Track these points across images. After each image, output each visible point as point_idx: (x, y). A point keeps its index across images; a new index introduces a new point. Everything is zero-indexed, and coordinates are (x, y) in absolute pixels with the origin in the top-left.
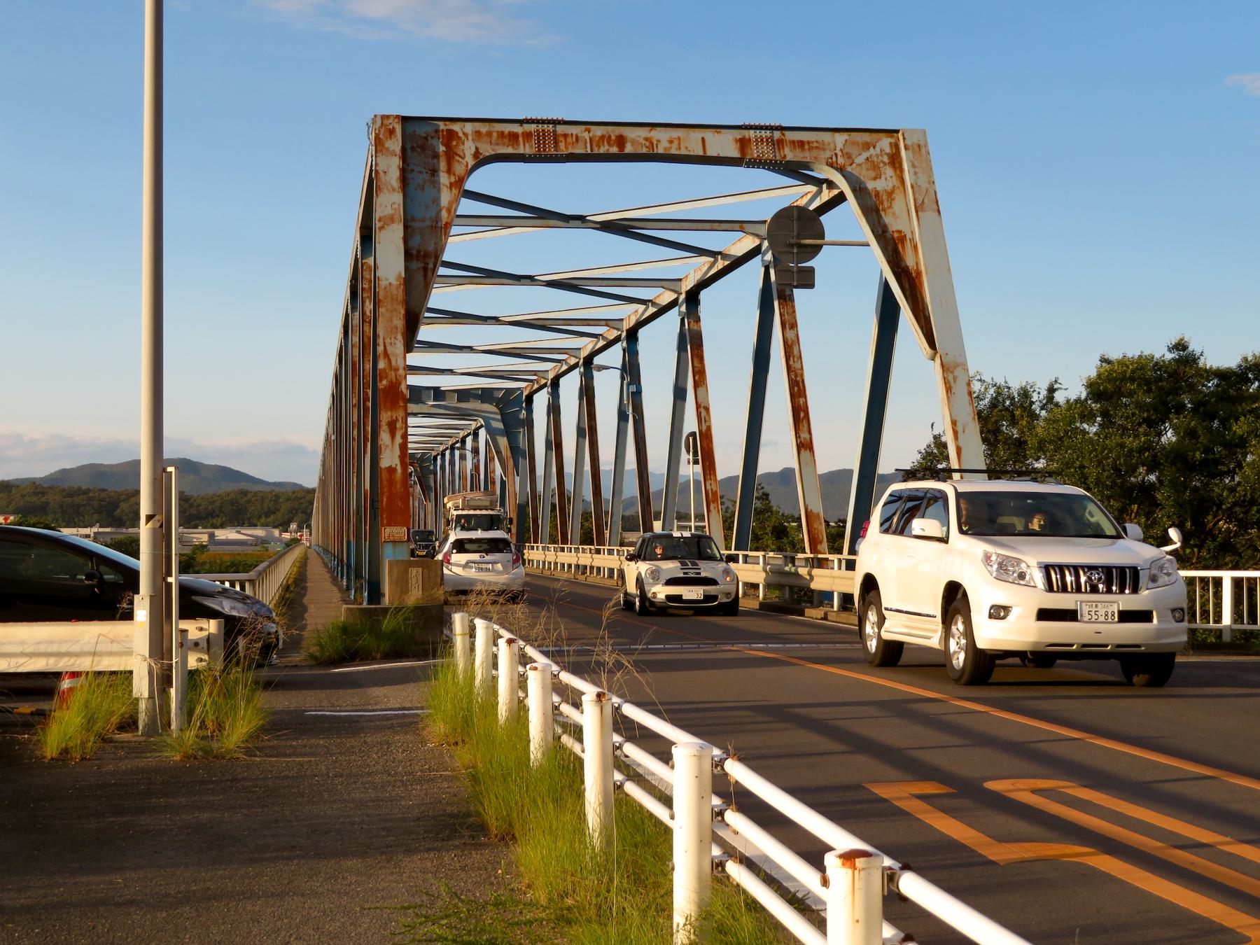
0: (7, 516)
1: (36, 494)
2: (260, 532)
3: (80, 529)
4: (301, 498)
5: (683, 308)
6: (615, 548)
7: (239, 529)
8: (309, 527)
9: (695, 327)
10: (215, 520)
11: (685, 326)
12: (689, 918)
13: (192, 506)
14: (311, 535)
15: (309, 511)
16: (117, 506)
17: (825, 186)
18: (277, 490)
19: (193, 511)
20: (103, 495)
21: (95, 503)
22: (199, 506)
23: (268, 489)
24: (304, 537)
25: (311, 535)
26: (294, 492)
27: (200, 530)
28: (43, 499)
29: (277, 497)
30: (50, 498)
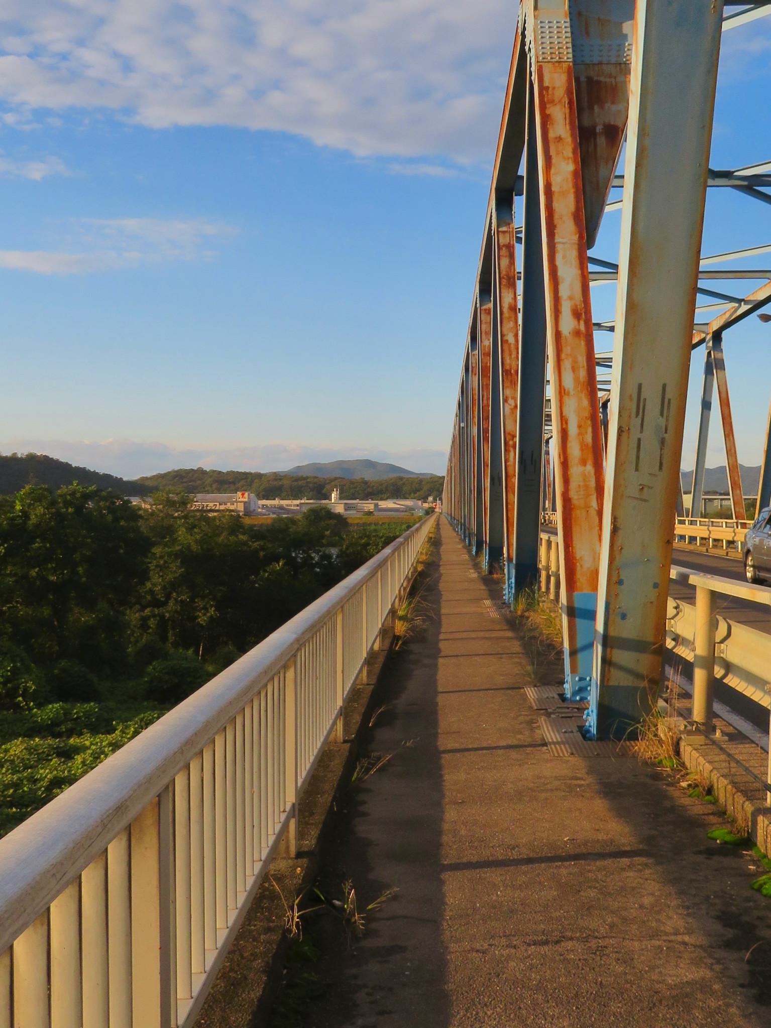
0: (243, 492)
1: (276, 480)
2: (409, 503)
3: (293, 501)
4: (435, 482)
5: (711, 344)
6: (698, 520)
7: (395, 501)
8: (441, 499)
9: (718, 355)
10: (383, 496)
11: (711, 357)
12: (509, 575)
13: (369, 487)
14: (442, 504)
15: (441, 490)
16: (324, 487)
17: (743, 303)
18: (421, 477)
19: (370, 490)
20: (315, 480)
21: (311, 485)
22: (373, 486)
23: (415, 476)
24: (438, 506)
25: (442, 504)
26: (431, 478)
27: (370, 501)
28: (280, 483)
29: (421, 481)
30: (285, 482)
